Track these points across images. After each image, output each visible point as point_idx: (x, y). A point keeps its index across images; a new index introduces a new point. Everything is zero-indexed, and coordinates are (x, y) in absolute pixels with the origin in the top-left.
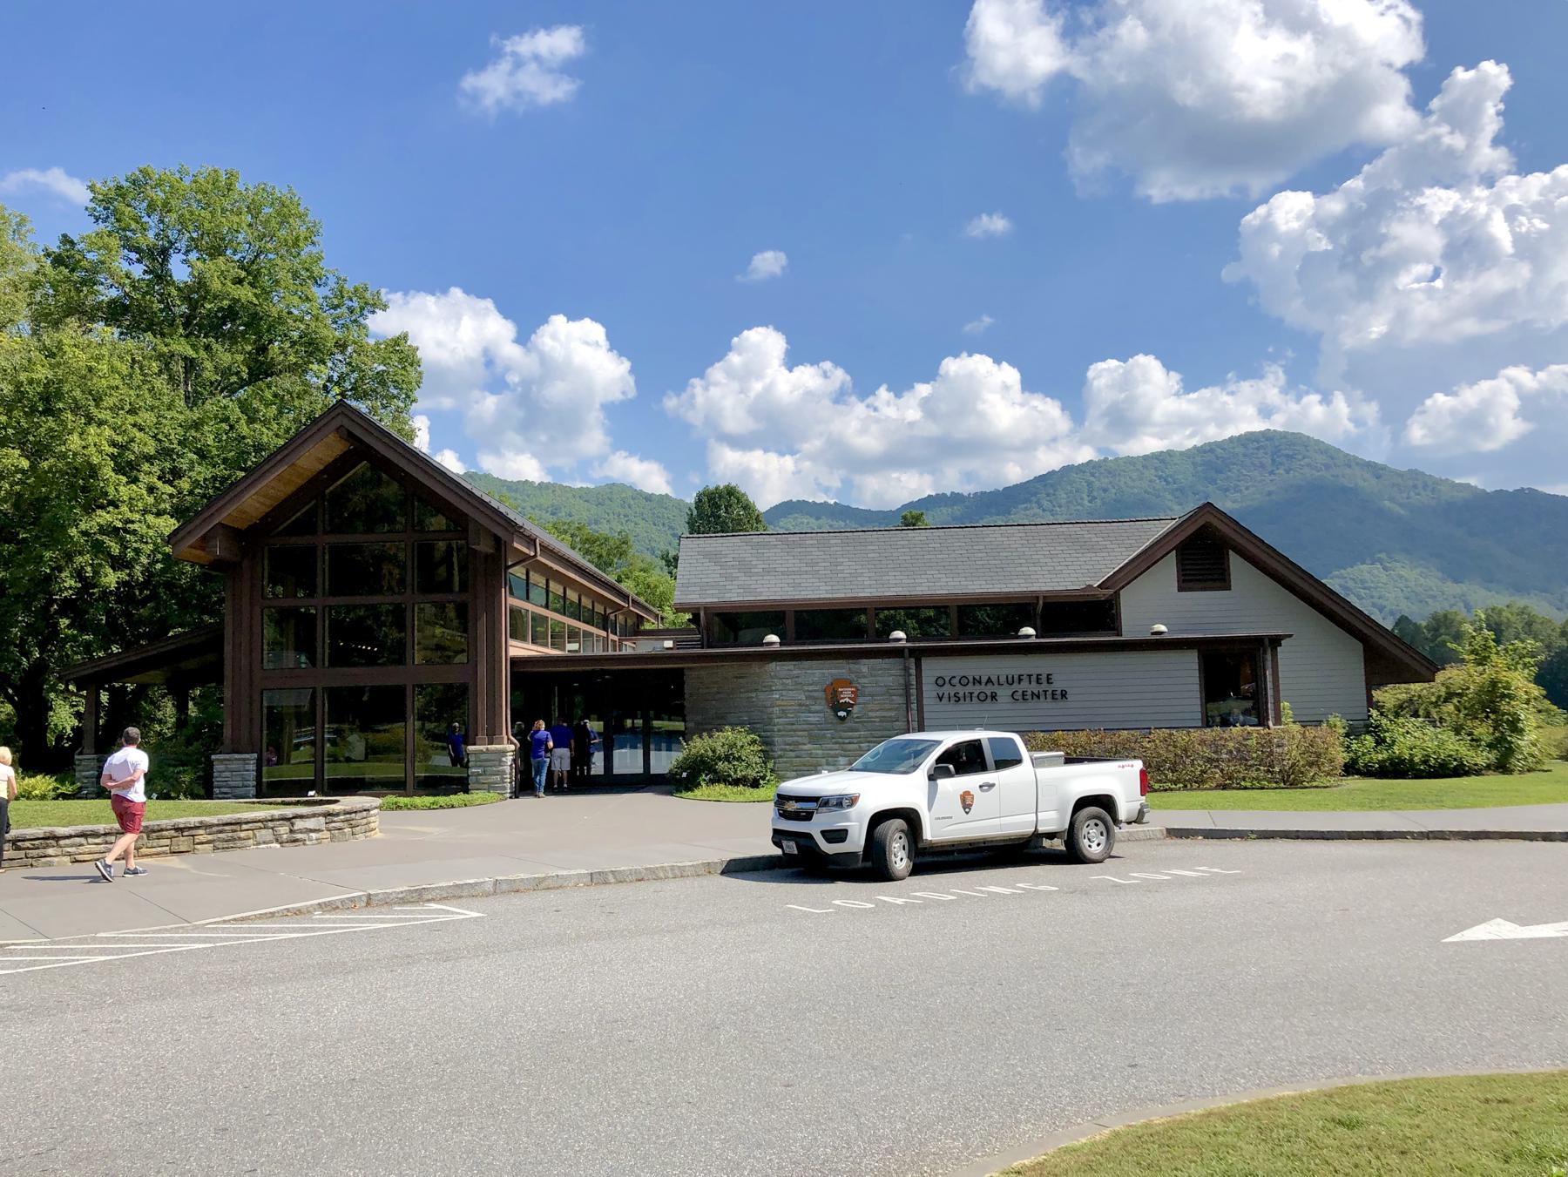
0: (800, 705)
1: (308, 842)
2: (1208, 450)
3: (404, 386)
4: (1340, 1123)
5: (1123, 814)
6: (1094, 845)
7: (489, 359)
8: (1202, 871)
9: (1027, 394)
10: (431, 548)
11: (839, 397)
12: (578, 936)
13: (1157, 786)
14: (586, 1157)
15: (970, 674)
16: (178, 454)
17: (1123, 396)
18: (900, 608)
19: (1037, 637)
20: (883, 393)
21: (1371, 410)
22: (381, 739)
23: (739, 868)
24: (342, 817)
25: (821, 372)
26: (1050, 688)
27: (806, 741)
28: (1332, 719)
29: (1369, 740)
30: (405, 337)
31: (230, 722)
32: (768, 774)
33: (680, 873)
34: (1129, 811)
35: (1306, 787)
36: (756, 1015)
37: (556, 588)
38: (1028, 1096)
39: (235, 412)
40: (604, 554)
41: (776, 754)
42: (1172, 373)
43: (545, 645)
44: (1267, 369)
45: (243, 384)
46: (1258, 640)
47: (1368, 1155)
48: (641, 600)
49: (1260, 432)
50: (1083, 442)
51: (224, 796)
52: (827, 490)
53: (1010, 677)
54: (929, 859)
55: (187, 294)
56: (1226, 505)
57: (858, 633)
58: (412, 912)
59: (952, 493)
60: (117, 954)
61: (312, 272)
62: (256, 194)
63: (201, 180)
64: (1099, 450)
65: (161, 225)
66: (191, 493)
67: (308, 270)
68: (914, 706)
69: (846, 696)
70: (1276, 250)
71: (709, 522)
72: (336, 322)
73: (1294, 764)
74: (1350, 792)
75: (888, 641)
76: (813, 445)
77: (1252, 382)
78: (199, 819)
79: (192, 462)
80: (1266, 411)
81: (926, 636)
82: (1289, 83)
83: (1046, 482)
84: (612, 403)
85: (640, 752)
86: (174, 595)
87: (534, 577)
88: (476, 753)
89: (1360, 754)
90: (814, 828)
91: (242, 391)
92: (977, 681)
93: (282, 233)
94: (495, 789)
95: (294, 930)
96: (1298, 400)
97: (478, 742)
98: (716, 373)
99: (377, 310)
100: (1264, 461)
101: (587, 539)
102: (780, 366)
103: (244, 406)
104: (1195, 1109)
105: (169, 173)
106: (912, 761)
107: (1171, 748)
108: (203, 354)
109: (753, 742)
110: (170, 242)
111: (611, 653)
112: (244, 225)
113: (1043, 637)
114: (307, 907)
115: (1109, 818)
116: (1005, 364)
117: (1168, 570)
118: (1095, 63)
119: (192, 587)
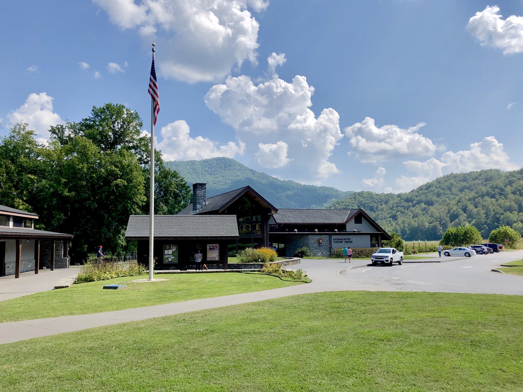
26: (350, 241)
49: (222, 157)
69: (321, 241)
90: (384, 260)
92: (340, 239)
117: (353, 221)
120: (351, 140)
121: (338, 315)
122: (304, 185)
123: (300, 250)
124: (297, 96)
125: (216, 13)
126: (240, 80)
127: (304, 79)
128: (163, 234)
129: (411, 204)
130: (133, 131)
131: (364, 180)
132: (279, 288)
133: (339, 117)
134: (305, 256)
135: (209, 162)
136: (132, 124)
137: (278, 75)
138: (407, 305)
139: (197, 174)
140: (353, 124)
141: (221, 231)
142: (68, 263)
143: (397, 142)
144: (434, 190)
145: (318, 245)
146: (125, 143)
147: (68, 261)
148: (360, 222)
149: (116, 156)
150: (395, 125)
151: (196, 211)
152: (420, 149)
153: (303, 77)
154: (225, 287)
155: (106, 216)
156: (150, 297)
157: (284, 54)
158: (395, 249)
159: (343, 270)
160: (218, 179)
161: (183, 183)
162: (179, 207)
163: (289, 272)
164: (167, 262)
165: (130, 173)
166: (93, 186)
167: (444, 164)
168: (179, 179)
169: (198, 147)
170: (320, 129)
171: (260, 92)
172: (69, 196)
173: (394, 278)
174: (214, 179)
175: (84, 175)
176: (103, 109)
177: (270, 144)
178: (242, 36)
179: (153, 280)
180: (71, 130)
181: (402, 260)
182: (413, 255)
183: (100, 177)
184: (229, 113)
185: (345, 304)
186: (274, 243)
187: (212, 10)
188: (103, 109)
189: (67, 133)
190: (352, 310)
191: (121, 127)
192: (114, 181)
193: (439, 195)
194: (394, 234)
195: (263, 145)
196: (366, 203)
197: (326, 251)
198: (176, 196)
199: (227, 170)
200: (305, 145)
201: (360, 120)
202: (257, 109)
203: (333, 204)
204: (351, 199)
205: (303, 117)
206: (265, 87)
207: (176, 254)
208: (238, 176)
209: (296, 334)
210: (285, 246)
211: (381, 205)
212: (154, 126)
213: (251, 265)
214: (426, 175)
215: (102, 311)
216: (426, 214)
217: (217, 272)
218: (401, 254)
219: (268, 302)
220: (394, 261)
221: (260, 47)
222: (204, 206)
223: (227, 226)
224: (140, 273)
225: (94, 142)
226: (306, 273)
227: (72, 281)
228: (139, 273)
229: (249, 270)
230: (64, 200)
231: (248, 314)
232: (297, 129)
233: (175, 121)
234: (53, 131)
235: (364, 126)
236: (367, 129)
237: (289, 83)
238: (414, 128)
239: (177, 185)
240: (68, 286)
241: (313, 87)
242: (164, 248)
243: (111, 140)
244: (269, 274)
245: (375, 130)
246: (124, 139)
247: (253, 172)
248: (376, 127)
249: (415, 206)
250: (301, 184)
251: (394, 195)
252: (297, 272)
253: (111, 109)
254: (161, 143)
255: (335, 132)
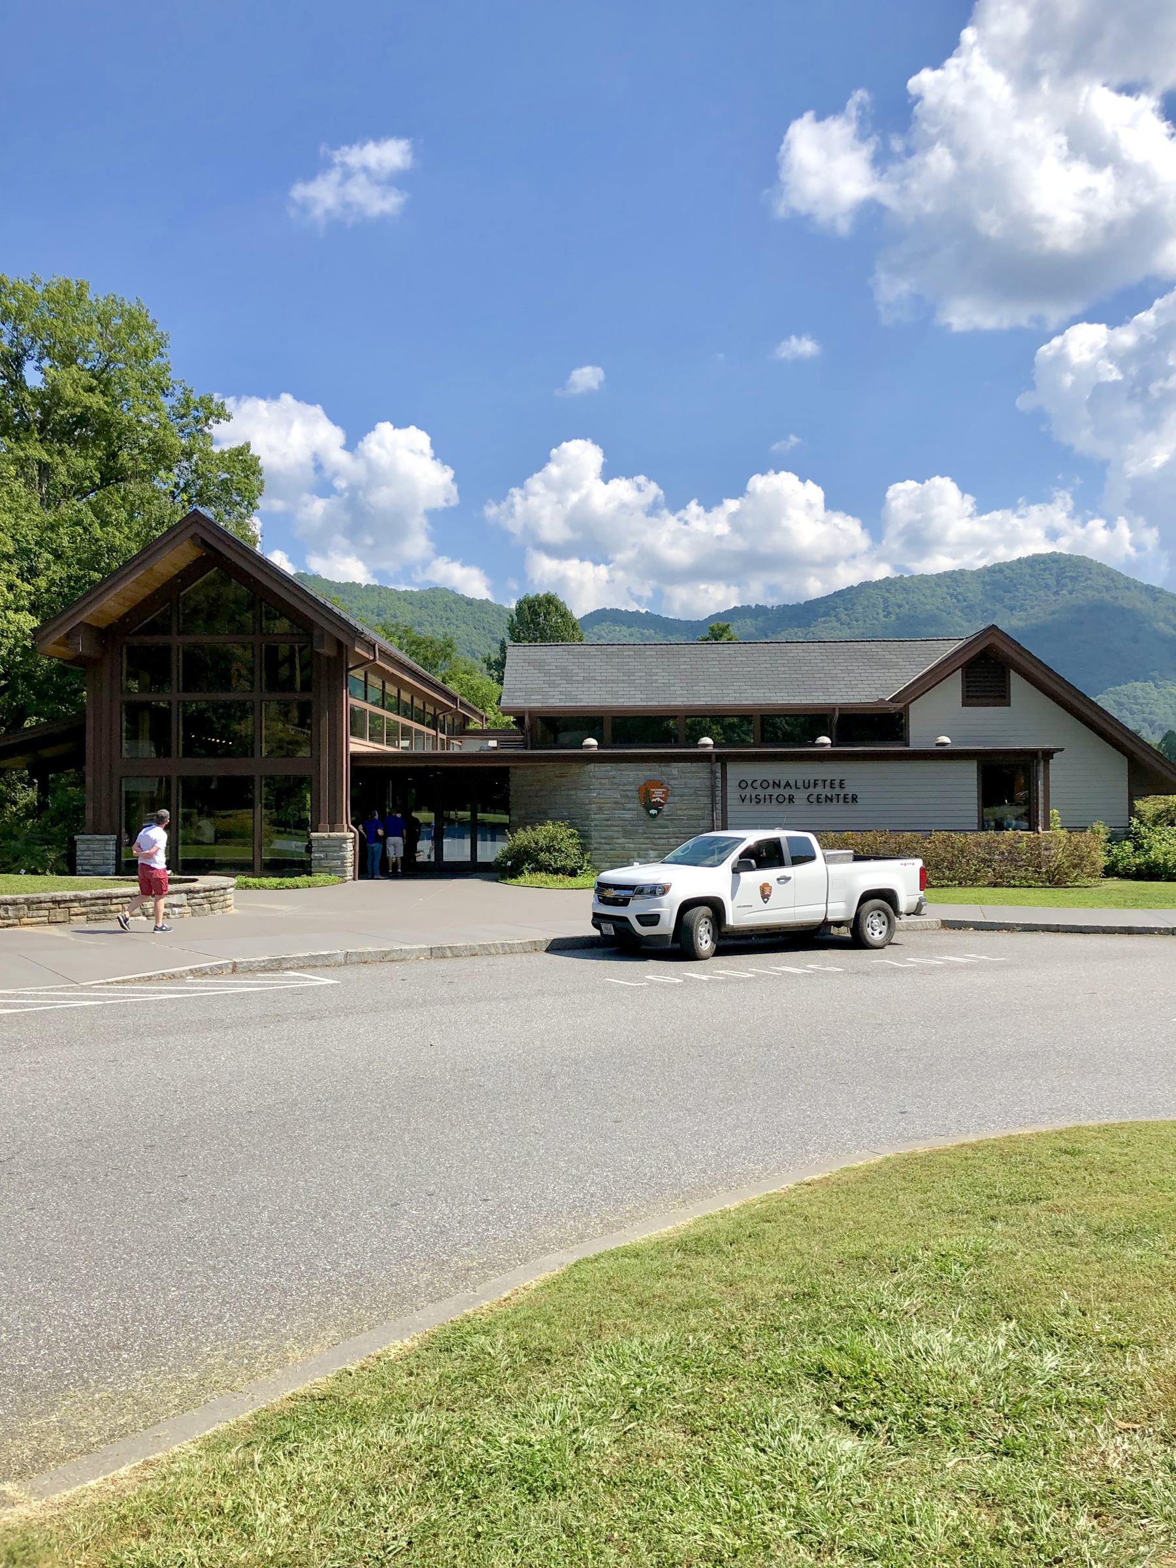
0: (616, 803)
1: (171, 916)
2: (997, 570)
3: (247, 494)
4: (1066, 1152)
5: (903, 907)
6: (876, 933)
7: (318, 465)
8: (971, 958)
9: (830, 512)
10: (276, 649)
11: (652, 510)
12: (425, 1001)
13: (934, 883)
14: (457, 1171)
15: (770, 778)
16: (35, 554)
17: (919, 516)
18: (706, 716)
19: (832, 745)
20: (694, 508)
21: (1151, 536)
22: (225, 824)
23: (560, 947)
24: (202, 894)
25: (635, 485)
27: (620, 835)
28: (1095, 826)
29: (1129, 846)
30: (248, 446)
31: (91, 805)
32: (585, 864)
33: (509, 950)
34: (909, 905)
35: (1068, 887)
36: (586, 1067)
37: (391, 689)
38: (816, 1133)
39: (89, 517)
40: (430, 656)
41: (592, 847)
42: (967, 496)
43: (381, 742)
44: (1056, 494)
45: (95, 488)
46: (1033, 754)
47: (1085, 1174)
48: (465, 700)
50: (880, 559)
51: (87, 873)
52: (638, 600)
53: (807, 781)
54: (731, 942)
55: (38, 398)
56: (1009, 623)
57: (667, 738)
58: (274, 979)
59: (757, 605)
60: (20, 1008)
61: (160, 382)
62: (107, 305)
63: (53, 289)
64: (896, 568)
65: (15, 333)
66: (48, 591)
67: (155, 380)
68: (719, 806)
69: (657, 795)
70: (1068, 380)
71: (529, 628)
72: (183, 431)
73: (1059, 866)
74: (1109, 891)
75: (697, 747)
76: (626, 555)
77: (1041, 506)
78: (74, 893)
79: (48, 562)
80: (1053, 534)
81: (730, 742)
82: (1089, 216)
83: (847, 597)
84: (436, 509)
85: (467, 842)
86: (30, 687)
87: (372, 679)
88: (318, 839)
89: (1120, 858)
90: (630, 912)
91: (93, 494)
92: (776, 785)
93: (132, 344)
94: (336, 872)
95: (171, 992)
96: (1084, 524)
97: (319, 829)
98: (535, 483)
99: (221, 420)
100: (1049, 581)
101: (413, 642)
102: (596, 478)
103: (98, 512)
104: (949, 1143)
105: (22, 282)
106: (716, 857)
107: (949, 849)
108: (57, 459)
109: (572, 836)
110: (24, 350)
111: (439, 751)
112: (95, 335)
113: (837, 746)
114: (180, 972)
115: (890, 910)
116: (809, 483)
117: (954, 686)
118: (903, 191)
119: (48, 679)
148: (1001, 697)
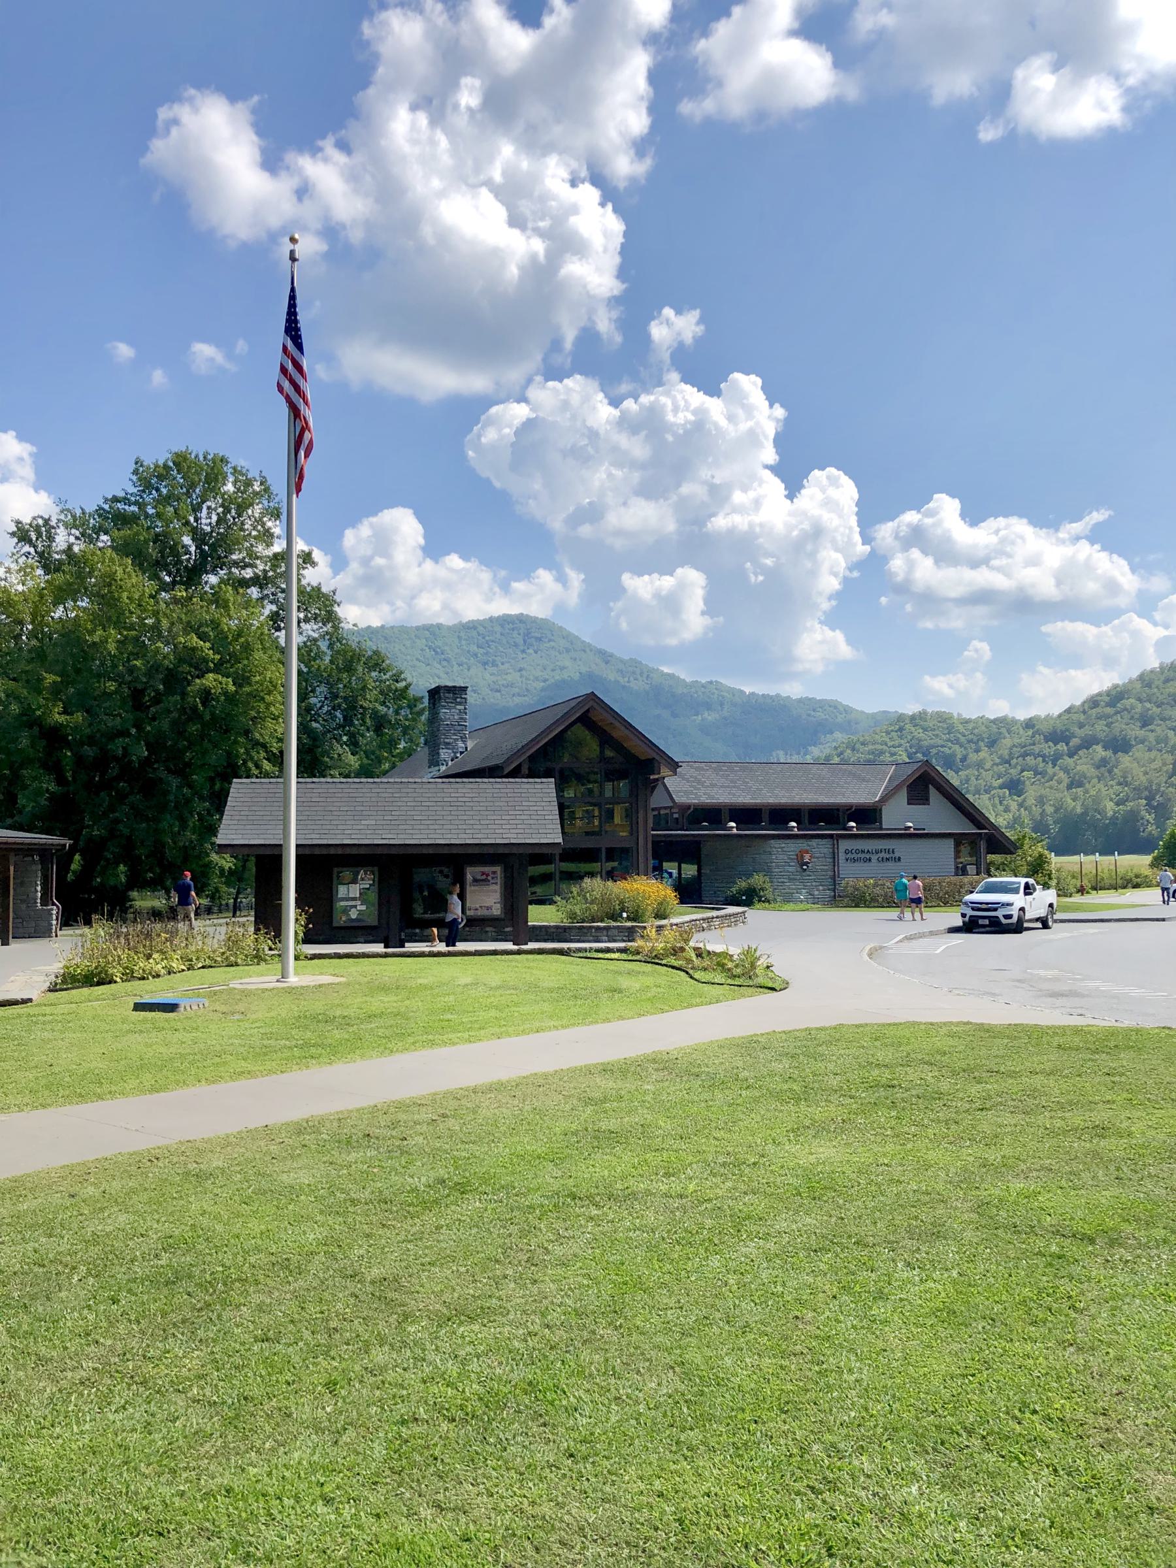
69: (807, 858)
90: (1000, 914)
92: (863, 852)
117: (903, 795)
120: (891, 562)
121: (894, 1114)
122: (753, 694)
123: (742, 884)
124: (733, 434)
125: (498, 192)
126: (569, 390)
127: (754, 384)
128: (333, 836)
129: (1065, 748)
130: (254, 533)
131: (927, 678)
132: (686, 1008)
133: (856, 496)
134: (760, 901)
135: (480, 629)
136: (250, 512)
137: (680, 373)
138: (1123, 1079)
139: (445, 663)
140: (897, 516)
141: (508, 827)
142: (54, 922)
143: (1025, 567)
144: (1133, 708)
145: (799, 869)
146: (231, 568)
147: (54, 917)
148: (924, 800)
149: (202, 607)
150: (1021, 516)
151: (437, 768)
152: (1091, 587)
153: (753, 377)
154: (516, 1005)
155: (174, 782)
156: (272, 1042)
157: (698, 311)
158: (1031, 881)
159: (876, 944)
160: (505, 677)
161: (402, 684)
162: (393, 756)
163: (715, 954)
164: (345, 922)
165: (244, 655)
166: (137, 695)
167: (1161, 632)
168: (390, 673)
169: (448, 586)
170: (803, 529)
171: (625, 424)
172: (68, 726)
173: (1042, 973)
174: (494, 678)
175: (109, 663)
176: (165, 466)
177: (655, 576)
178: (575, 258)
179: (293, 980)
180: (73, 531)
181: (1053, 913)
182: (1077, 899)
183: (154, 669)
184: (537, 486)
185: (912, 1074)
186: (667, 861)
187: (489, 184)
188: (165, 466)
189: (62, 539)
190: (940, 1095)
191: (219, 522)
192: (198, 681)
193: (1146, 722)
194: (1024, 837)
195: (635, 577)
196: (933, 747)
197: (821, 888)
198: (380, 723)
199: (531, 651)
200: (756, 576)
201: (919, 502)
202: (618, 473)
203: (836, 748)
204: (888, 733)
205: (752, 494)
206: (642, 407)
207: (373, 896)
208: (562, 668)
209: (760, 1205)
210: (699, 870)
211: (977, 751)
212: (295, 496)
213: (598, 928)
214: (1109, 661)
215: (100, 1097)
216: (1109, 778)
217: (494, 953)
218: (1050, 896)
219: (654, 1061)
220: (1027, 917)
221: (626, 291)
222: (461, 753)
223: (525, 812)
224: (258, 958)
225: (141, 565)
226: (770, 960)
227: (45, 981)
228: (256, 957)
229: (591, 949)
230: (54, 736)
231: (589, 1110)
232: (731, 531)
233: (381, 510)
234: (22, 534)
235: (928, 521)
236: (939, 531)
237: (712, 396)
238: (1076, 527)
239: (381, 692)
240: (30, 1000)
241: (782, 406)
242: (335, 876)
243: (188, 560)
244: (654, 959)
245: (965, 535)
246: (226, 557)
247: (605, 657)
248: (965, 522)
249: (1075, 753)
250: (742, 692)
251: (1014, 722)
252: (743, 957)
253: (189, 467)
254: (342, 573)
255: (846, 540)
